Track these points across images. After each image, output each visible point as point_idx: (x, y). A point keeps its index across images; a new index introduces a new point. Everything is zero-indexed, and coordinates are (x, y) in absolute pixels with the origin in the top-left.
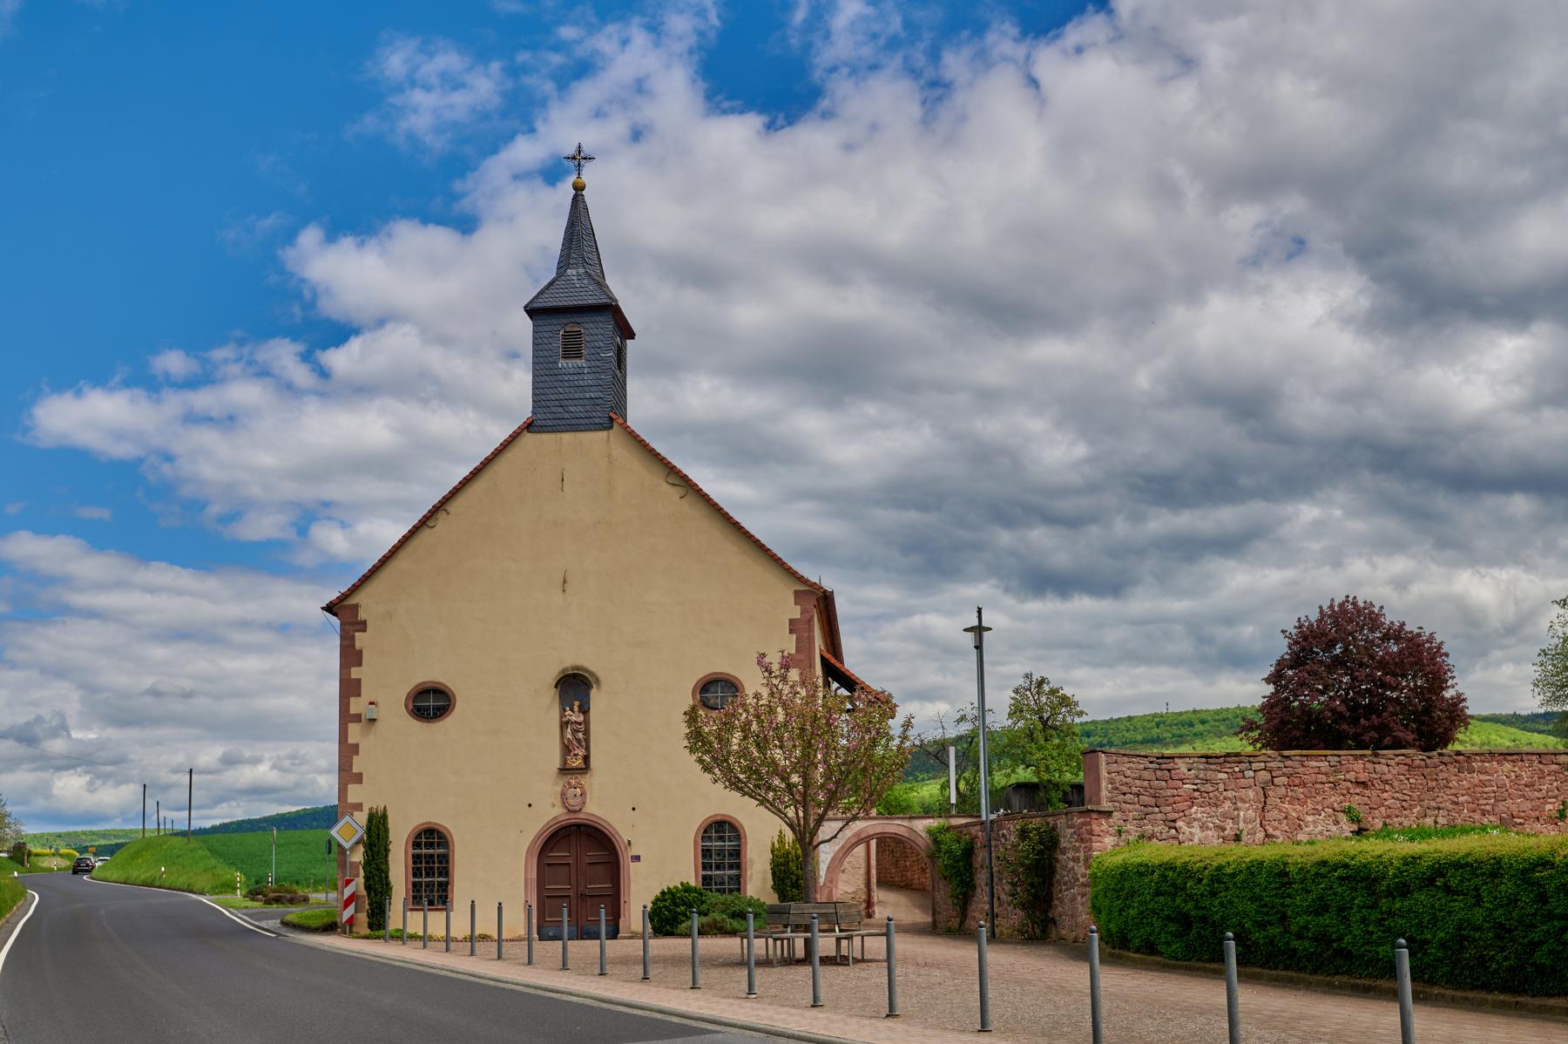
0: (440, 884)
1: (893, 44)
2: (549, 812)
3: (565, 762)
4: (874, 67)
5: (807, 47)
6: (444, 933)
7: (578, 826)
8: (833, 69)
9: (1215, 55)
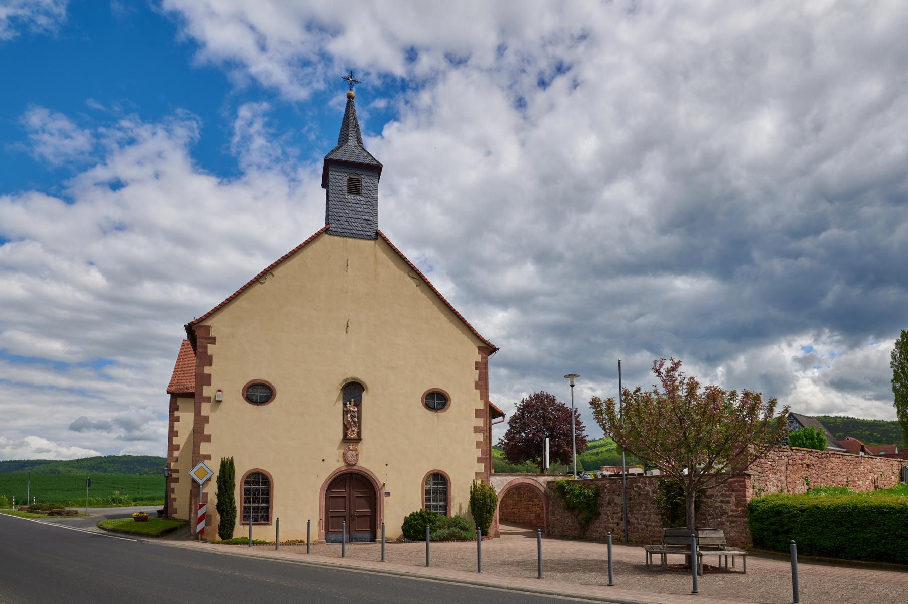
0: (263, 508)
1: (277, 160)
2: (335, 465)
3: (345, 435)
4: (269, 168)
5: (239, 153)
6: (275, 541)
7: (351, 474)
8: (250, 165)
9: (404, 190)
